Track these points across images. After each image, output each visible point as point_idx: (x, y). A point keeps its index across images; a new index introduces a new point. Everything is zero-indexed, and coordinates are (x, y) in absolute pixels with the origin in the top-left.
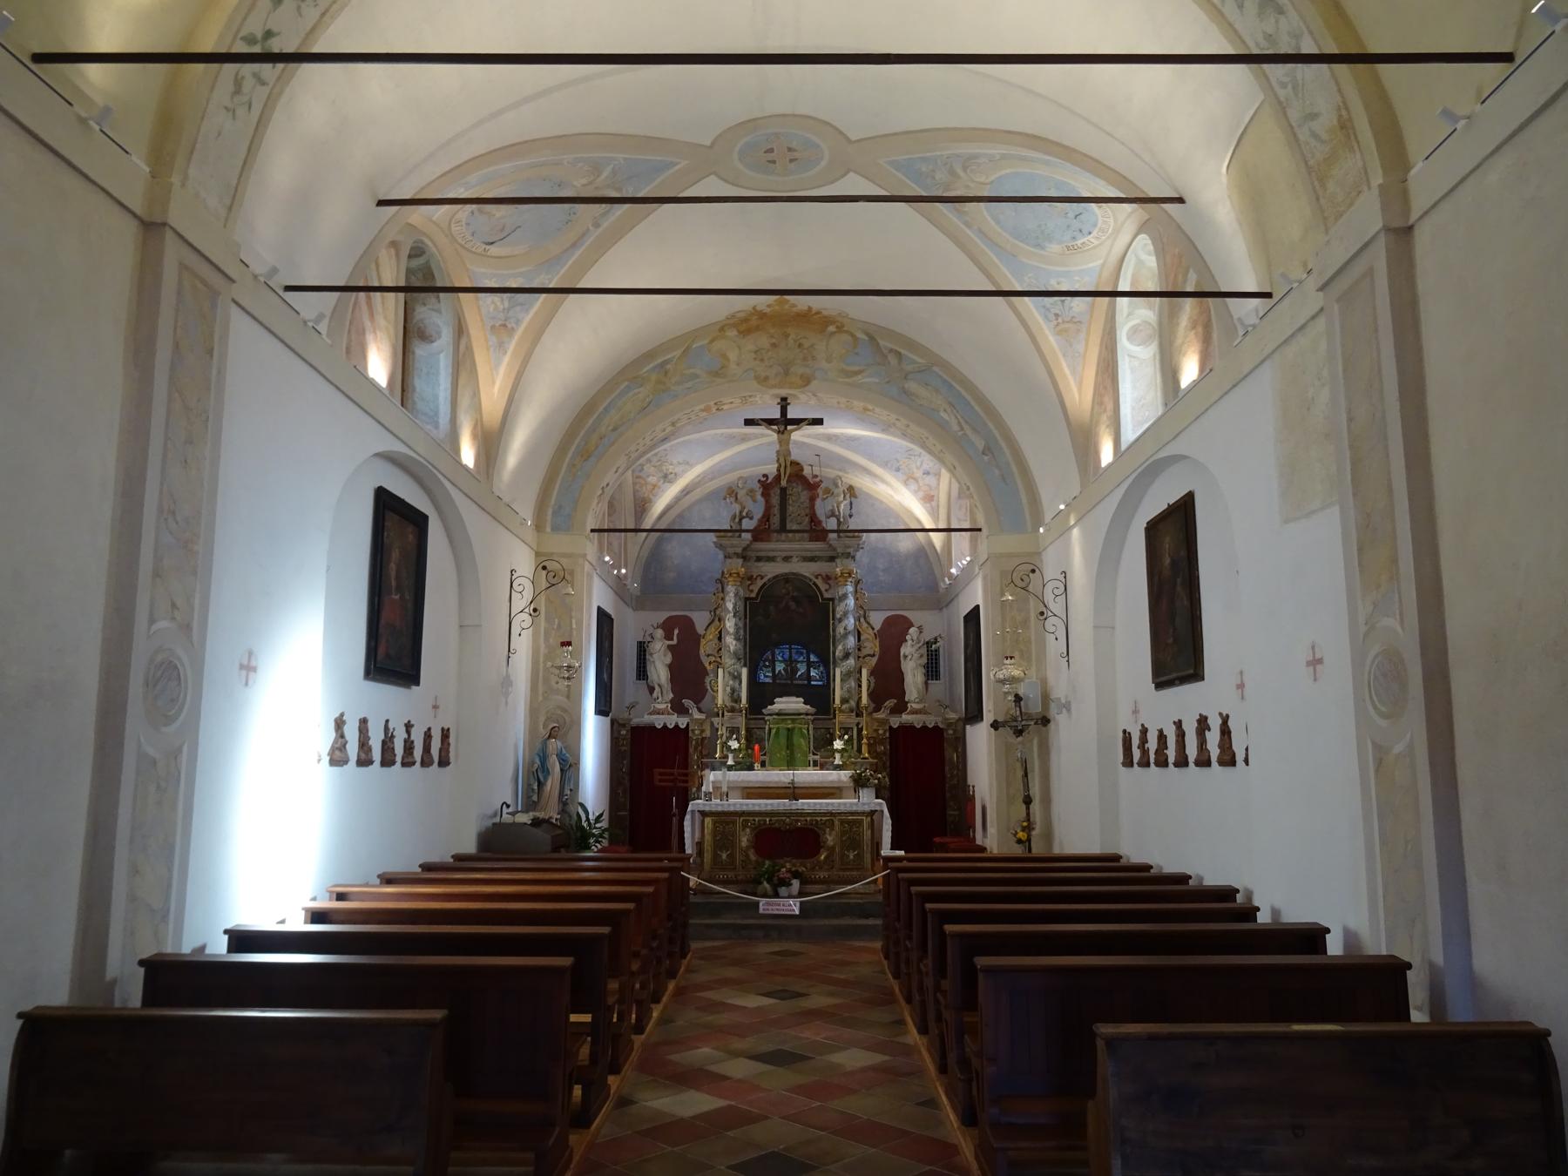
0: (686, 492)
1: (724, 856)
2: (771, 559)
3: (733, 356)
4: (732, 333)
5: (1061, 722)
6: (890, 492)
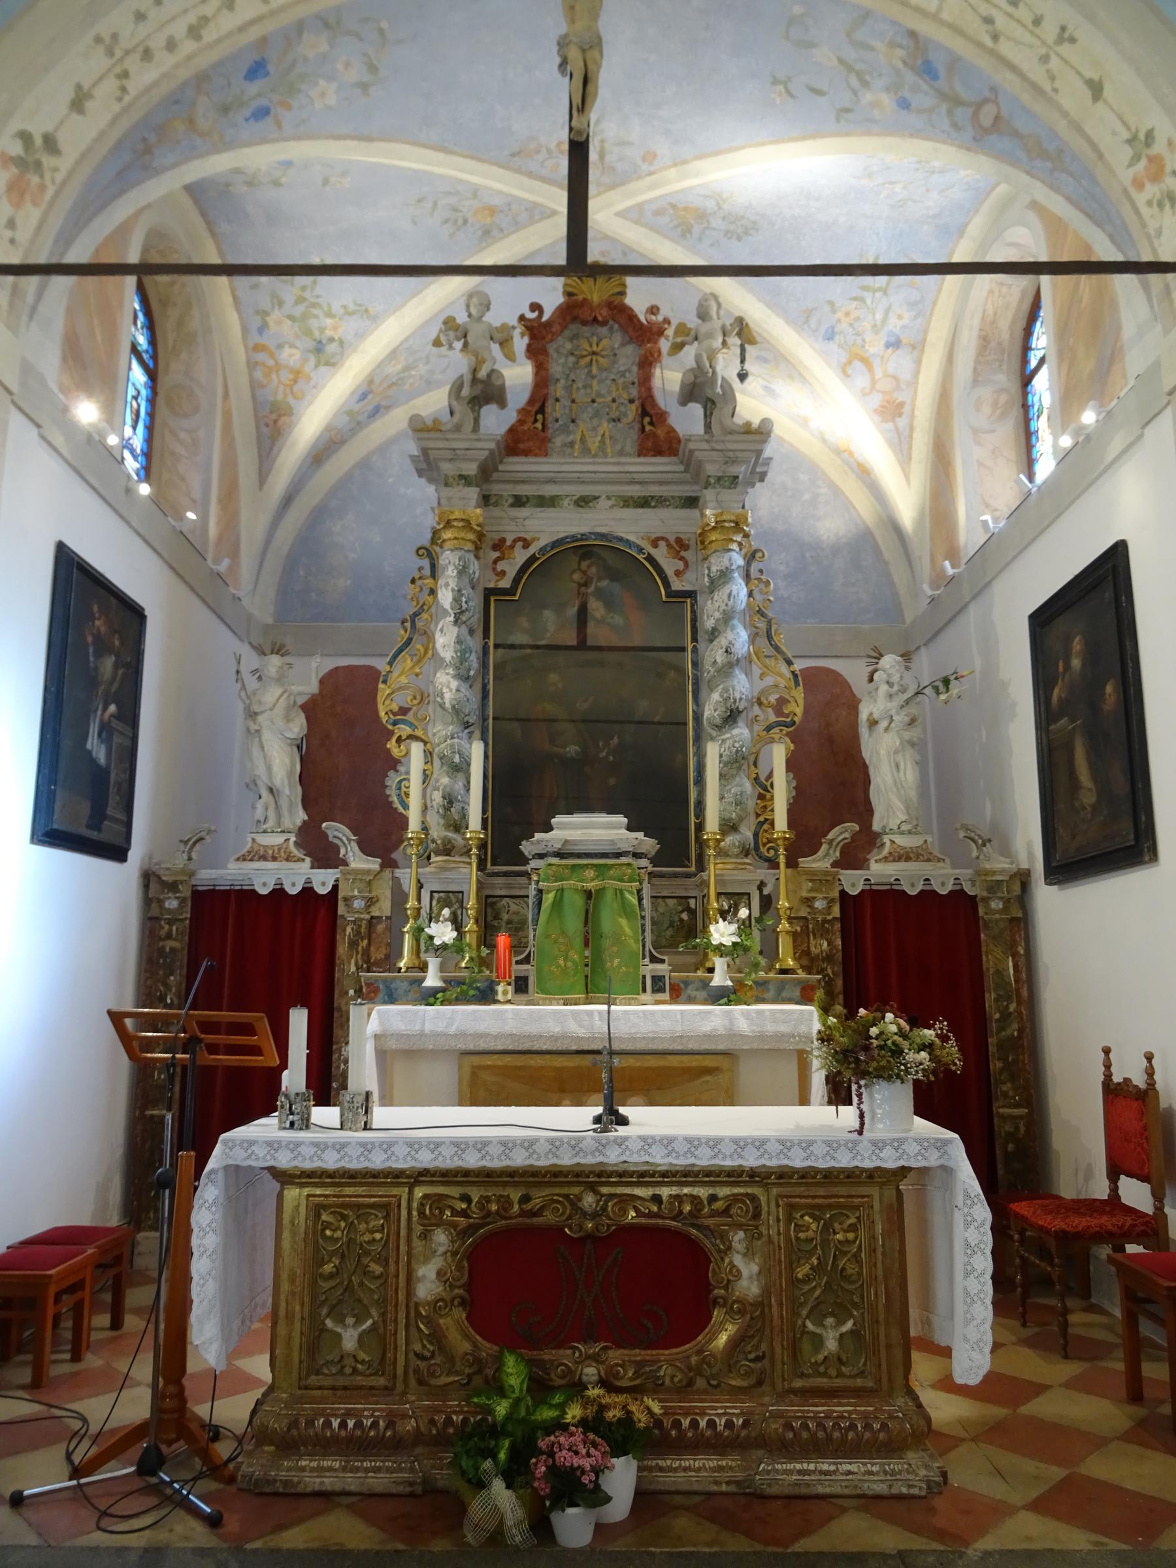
1: (350, 1339)
2: (546, 502)
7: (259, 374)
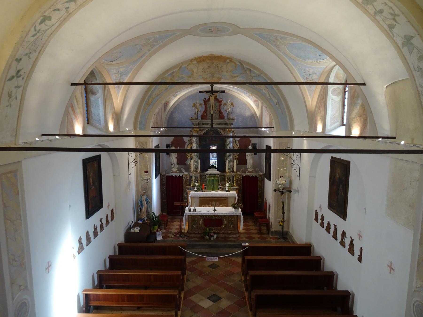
1: (195, 226)
3: (195, 70)
4: (195, 62)
5: (295, 197)
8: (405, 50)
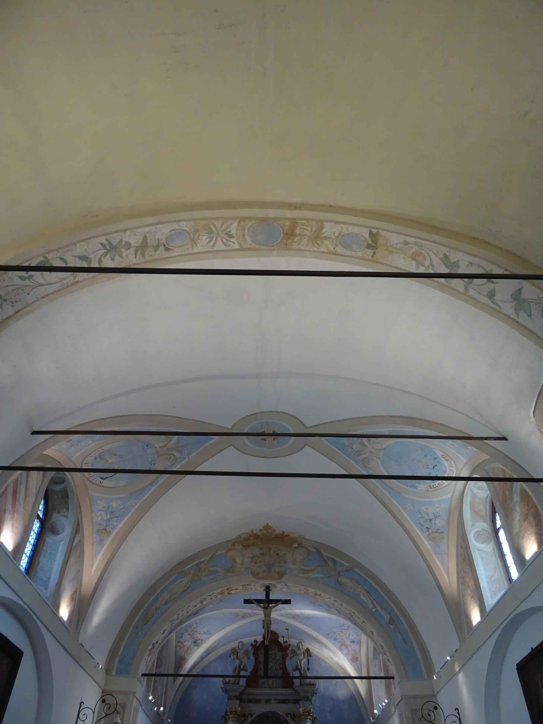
0: (207, 653)
2: (258, 701)
3: (239, 560)
4: (239, 547)
6: (331, 655)
7: (178, 649)
8: (523, 318)
